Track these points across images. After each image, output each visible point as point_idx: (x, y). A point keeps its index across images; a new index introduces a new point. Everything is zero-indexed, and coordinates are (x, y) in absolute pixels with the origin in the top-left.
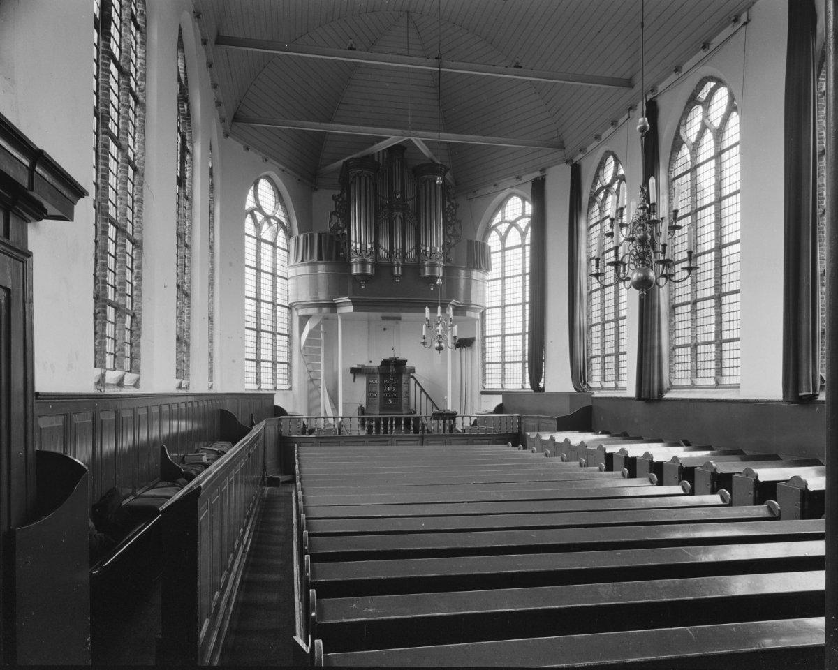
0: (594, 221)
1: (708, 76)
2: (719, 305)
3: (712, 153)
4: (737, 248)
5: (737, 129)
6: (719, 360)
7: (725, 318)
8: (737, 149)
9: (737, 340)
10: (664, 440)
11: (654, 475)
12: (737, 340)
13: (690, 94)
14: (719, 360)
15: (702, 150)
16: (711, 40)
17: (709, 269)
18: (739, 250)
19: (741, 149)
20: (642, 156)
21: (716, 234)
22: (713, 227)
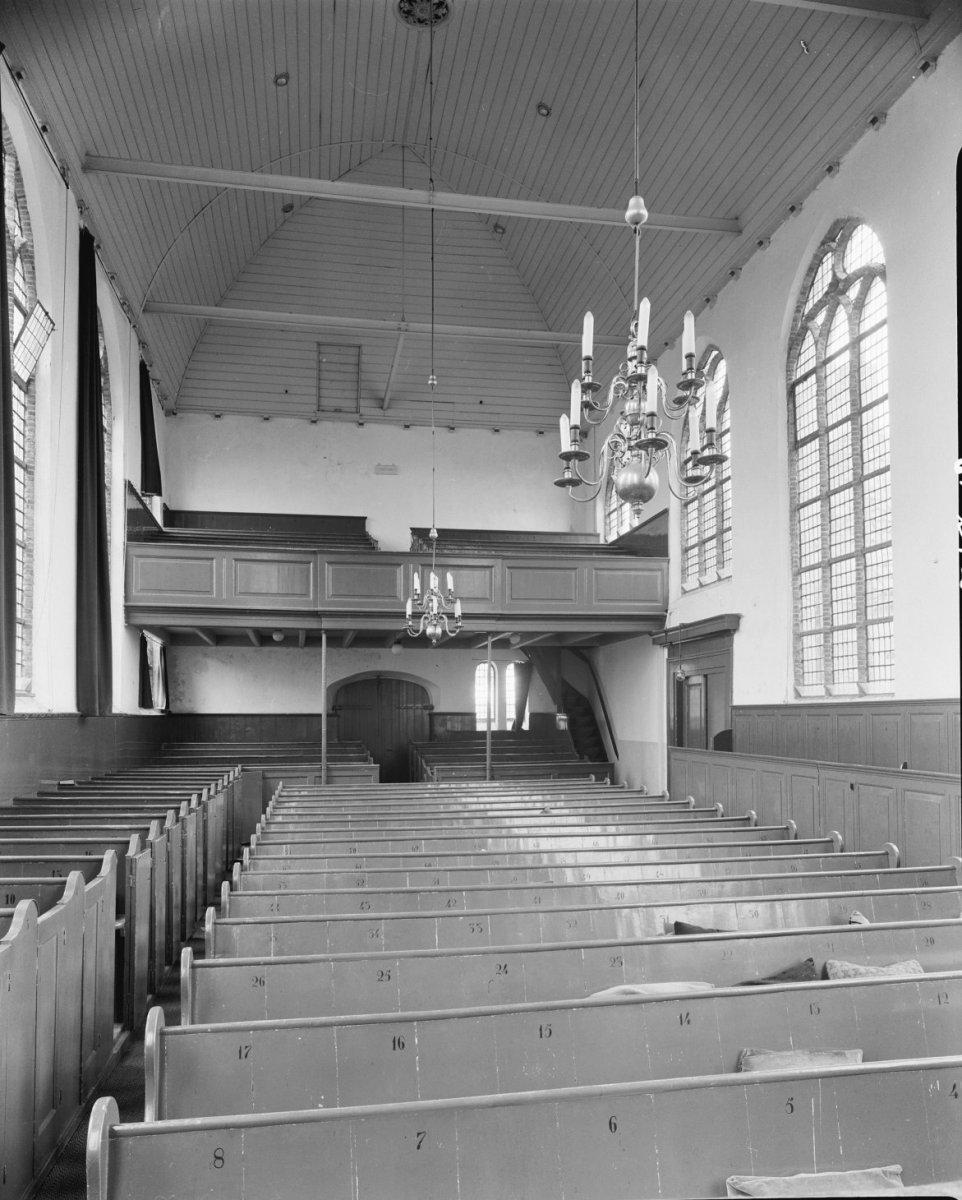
0: (613, 508)
1: (787, 347)
2: (864, 639)
3: (846, 340)
4: (885, 406)
5: (884, 298)
6: (864, 655)
7: (871, 586)
8: (884, 331)
9: (888, 545)
10: (856, 212)
11: (792, 822)
12: (888, 545)
13: (691, 430)
14: (864, 655)
15: (834, 336)
16: (887, 109)
17: (840, 615)
18: (889, 496)
19: (890, 335)
20: (517, 688)
21: (857, 518)
22: (851, 521)
